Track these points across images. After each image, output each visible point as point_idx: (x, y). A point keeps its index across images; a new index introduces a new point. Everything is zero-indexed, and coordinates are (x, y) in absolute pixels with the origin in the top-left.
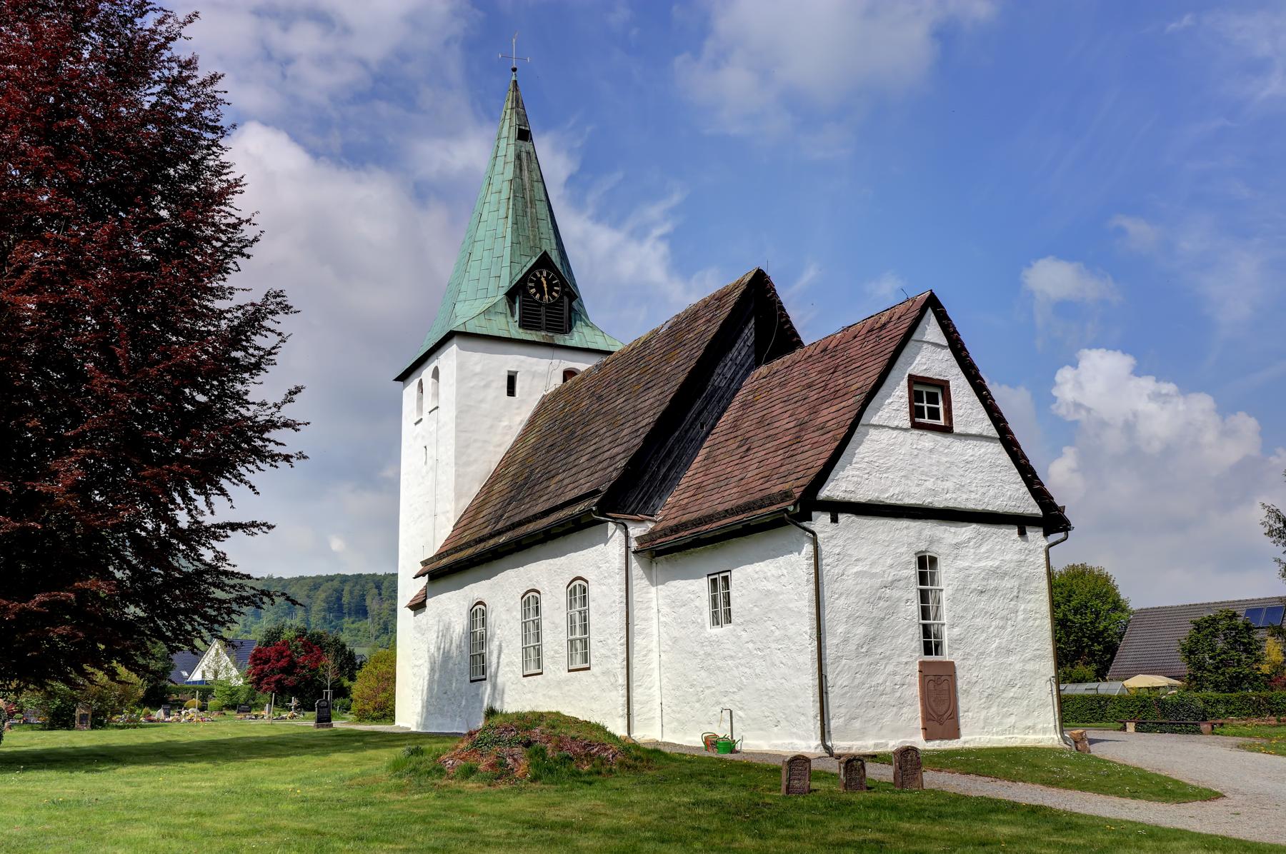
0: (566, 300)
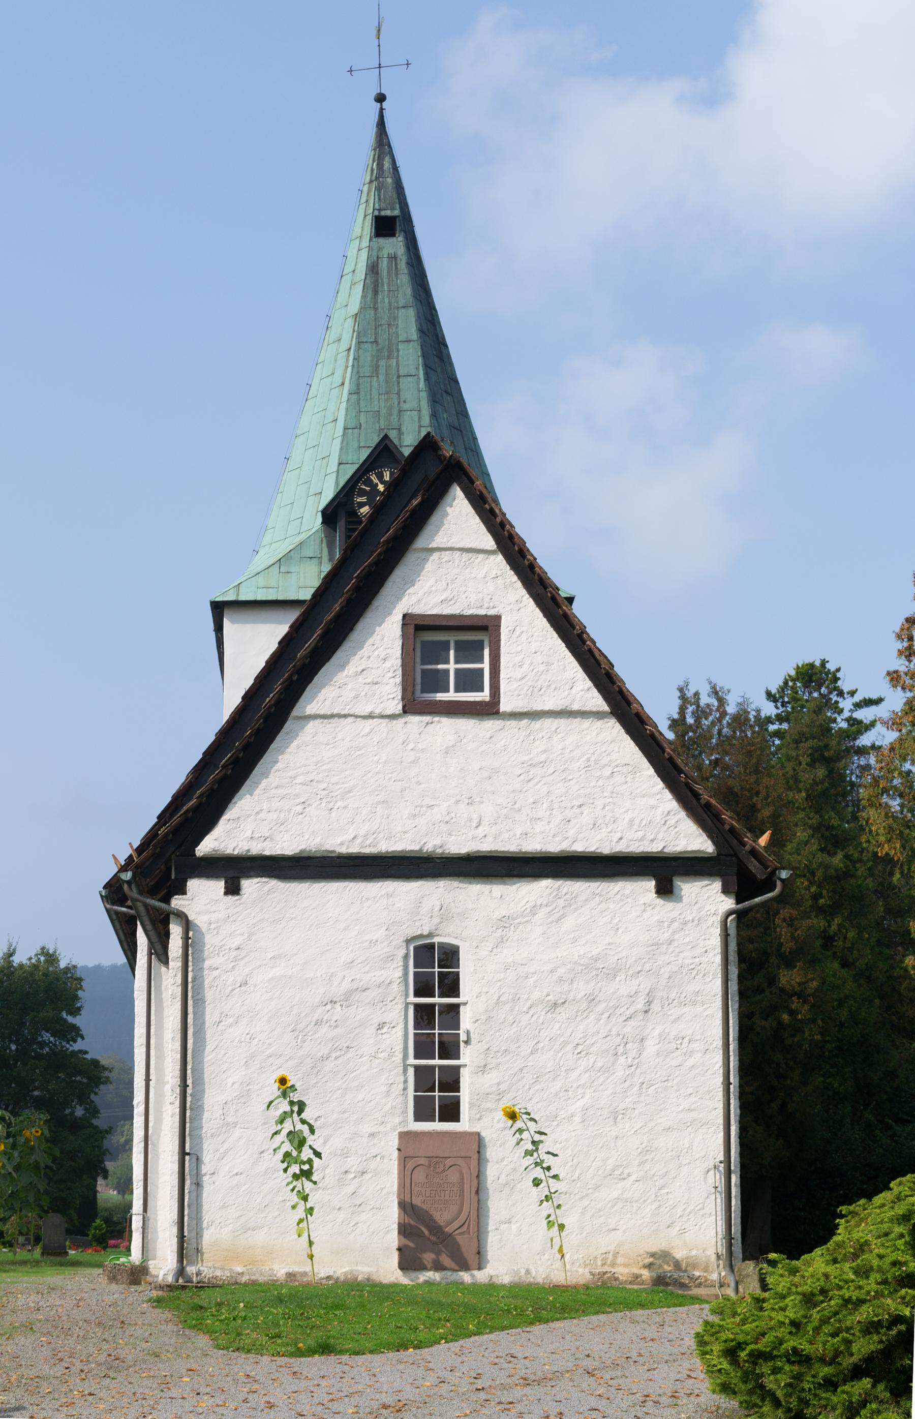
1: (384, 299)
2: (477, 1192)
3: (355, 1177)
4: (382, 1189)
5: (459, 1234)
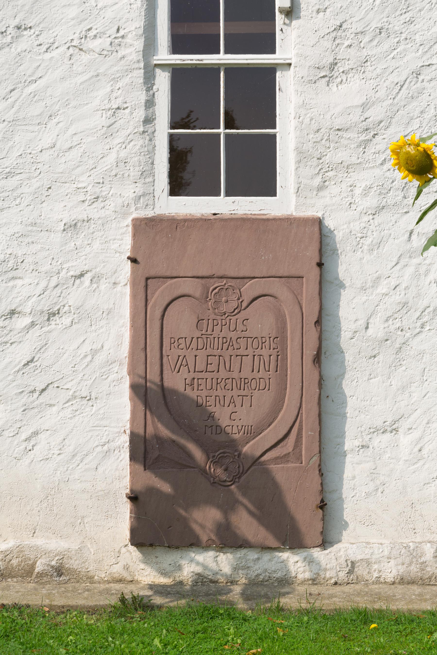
2: (317, 359)
3: (33, 324)
4: (94, 352)
5: (277, 460)
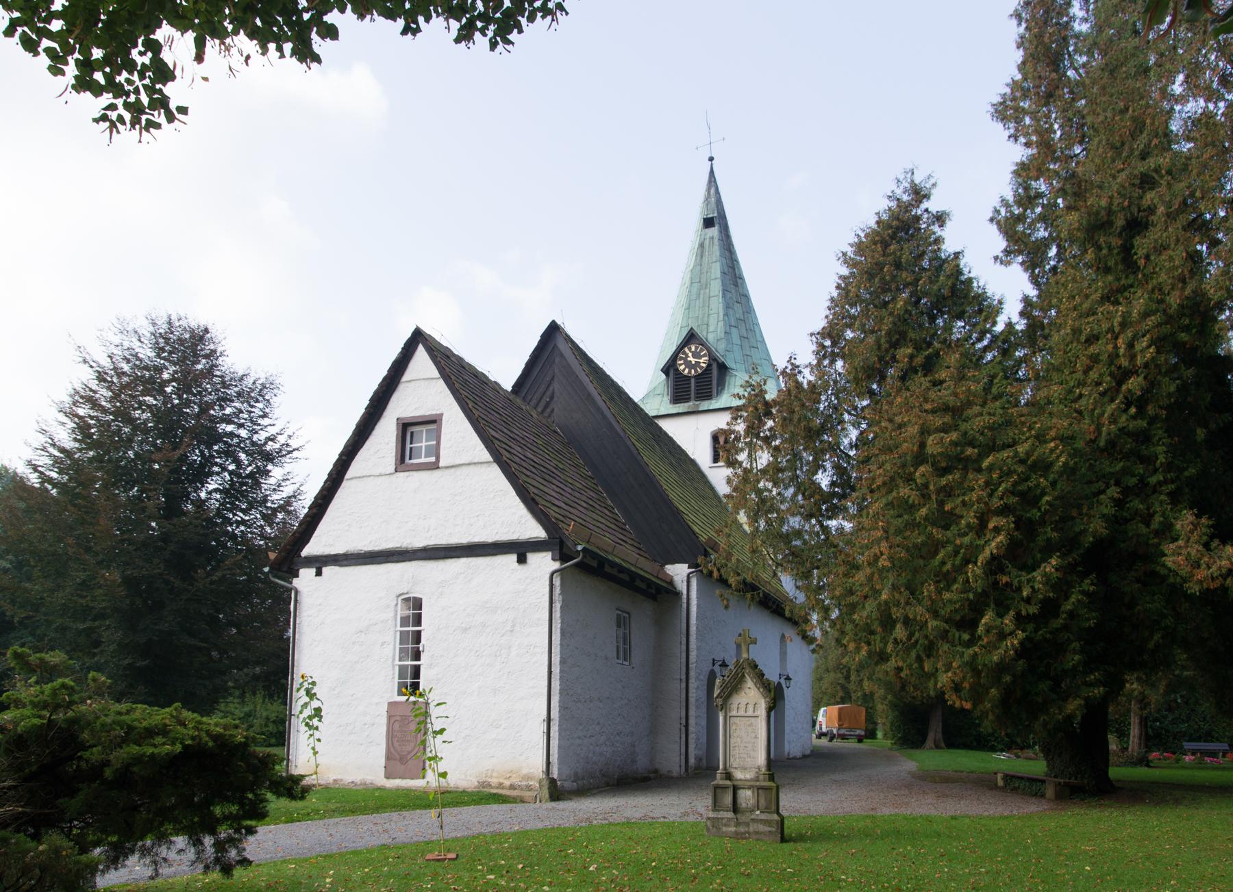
0: (715, 366)
1: (705, 260)
